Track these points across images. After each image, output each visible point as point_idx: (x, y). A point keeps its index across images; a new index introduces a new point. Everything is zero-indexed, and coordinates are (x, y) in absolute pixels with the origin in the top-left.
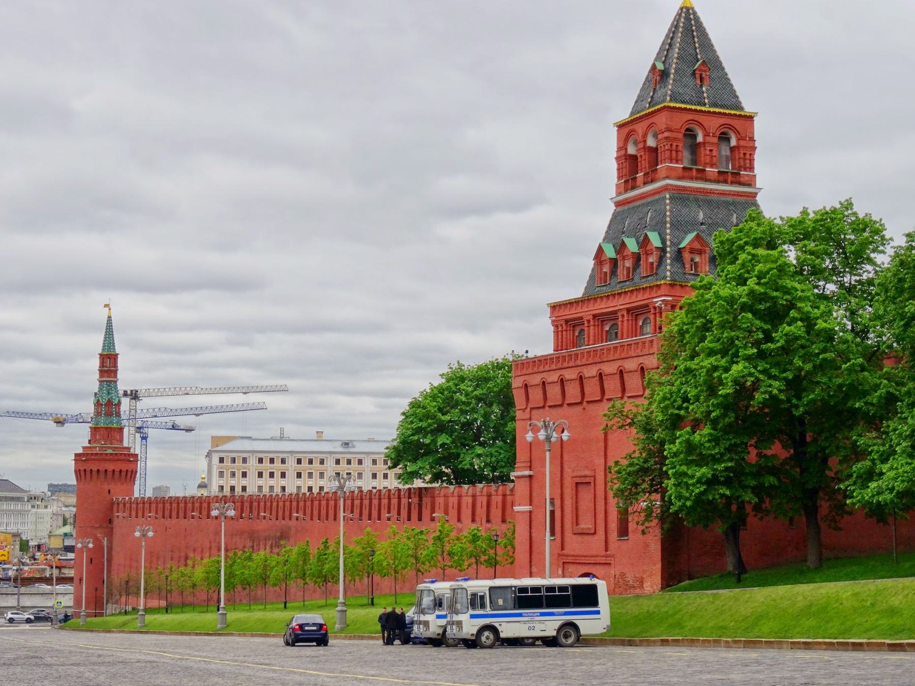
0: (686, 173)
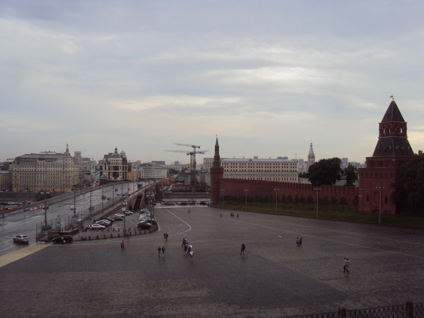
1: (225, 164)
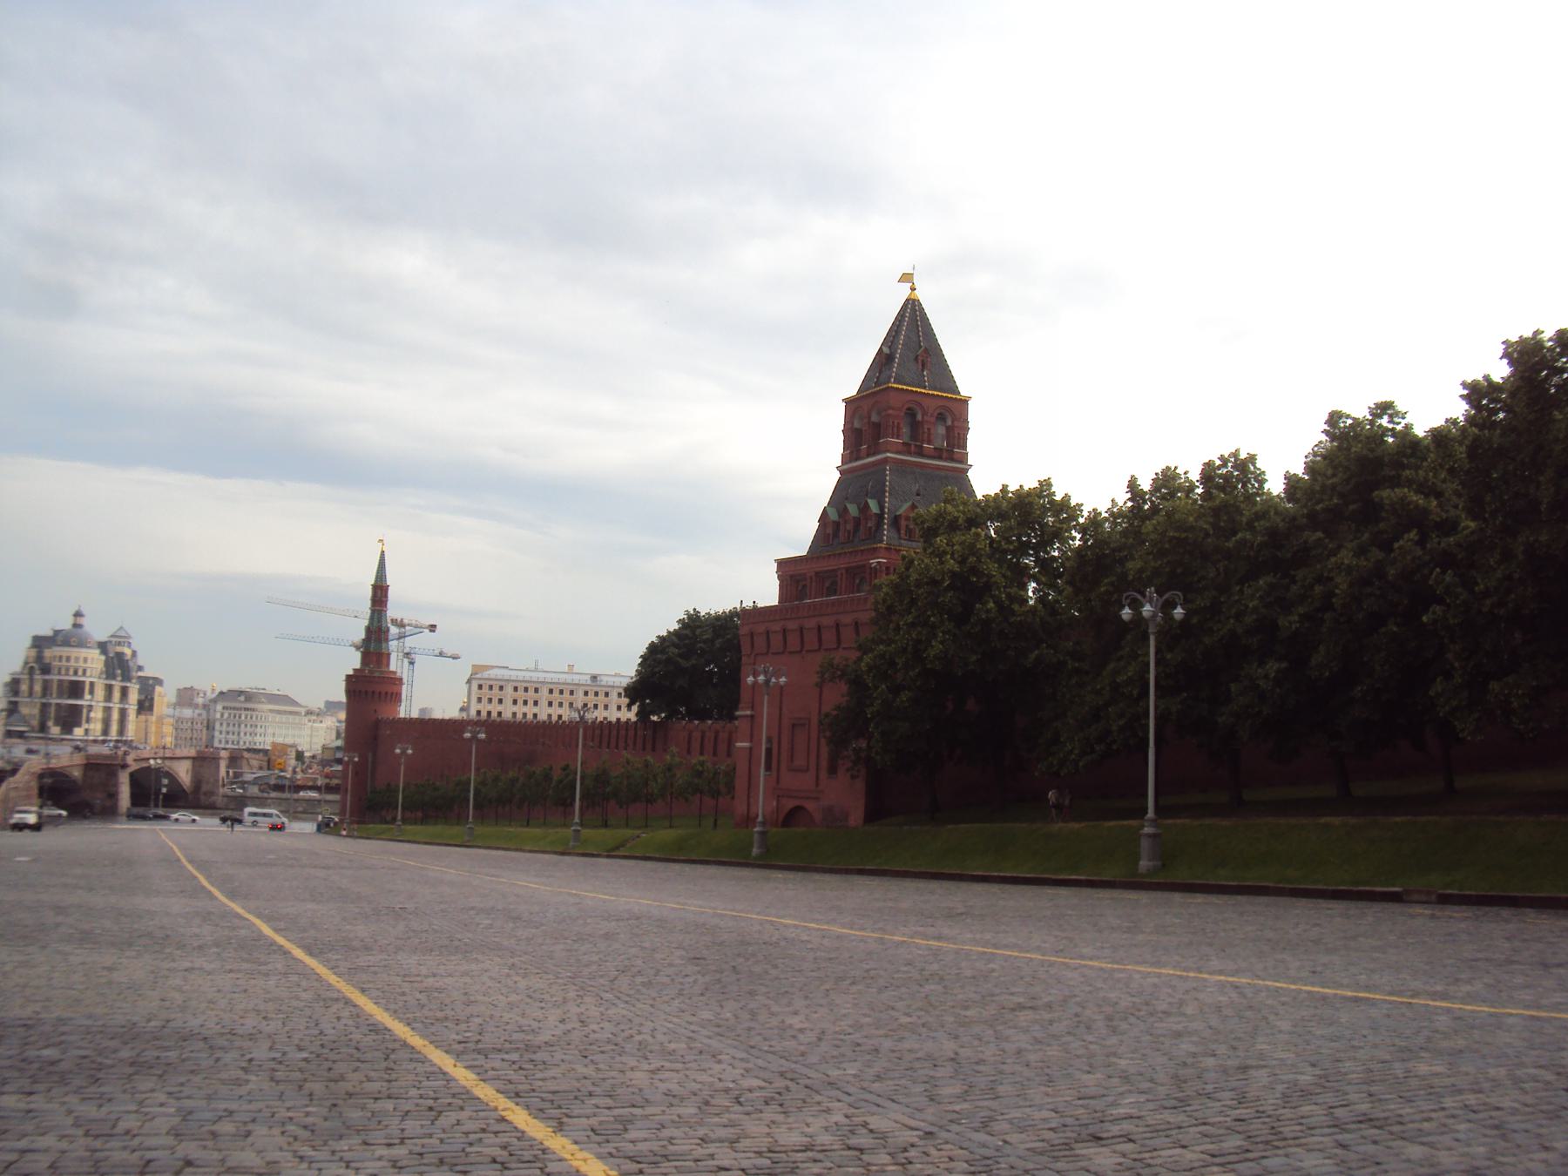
0: (906, 449)
1: (526, 690)
